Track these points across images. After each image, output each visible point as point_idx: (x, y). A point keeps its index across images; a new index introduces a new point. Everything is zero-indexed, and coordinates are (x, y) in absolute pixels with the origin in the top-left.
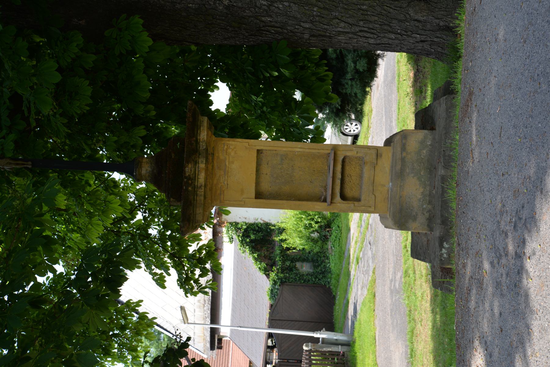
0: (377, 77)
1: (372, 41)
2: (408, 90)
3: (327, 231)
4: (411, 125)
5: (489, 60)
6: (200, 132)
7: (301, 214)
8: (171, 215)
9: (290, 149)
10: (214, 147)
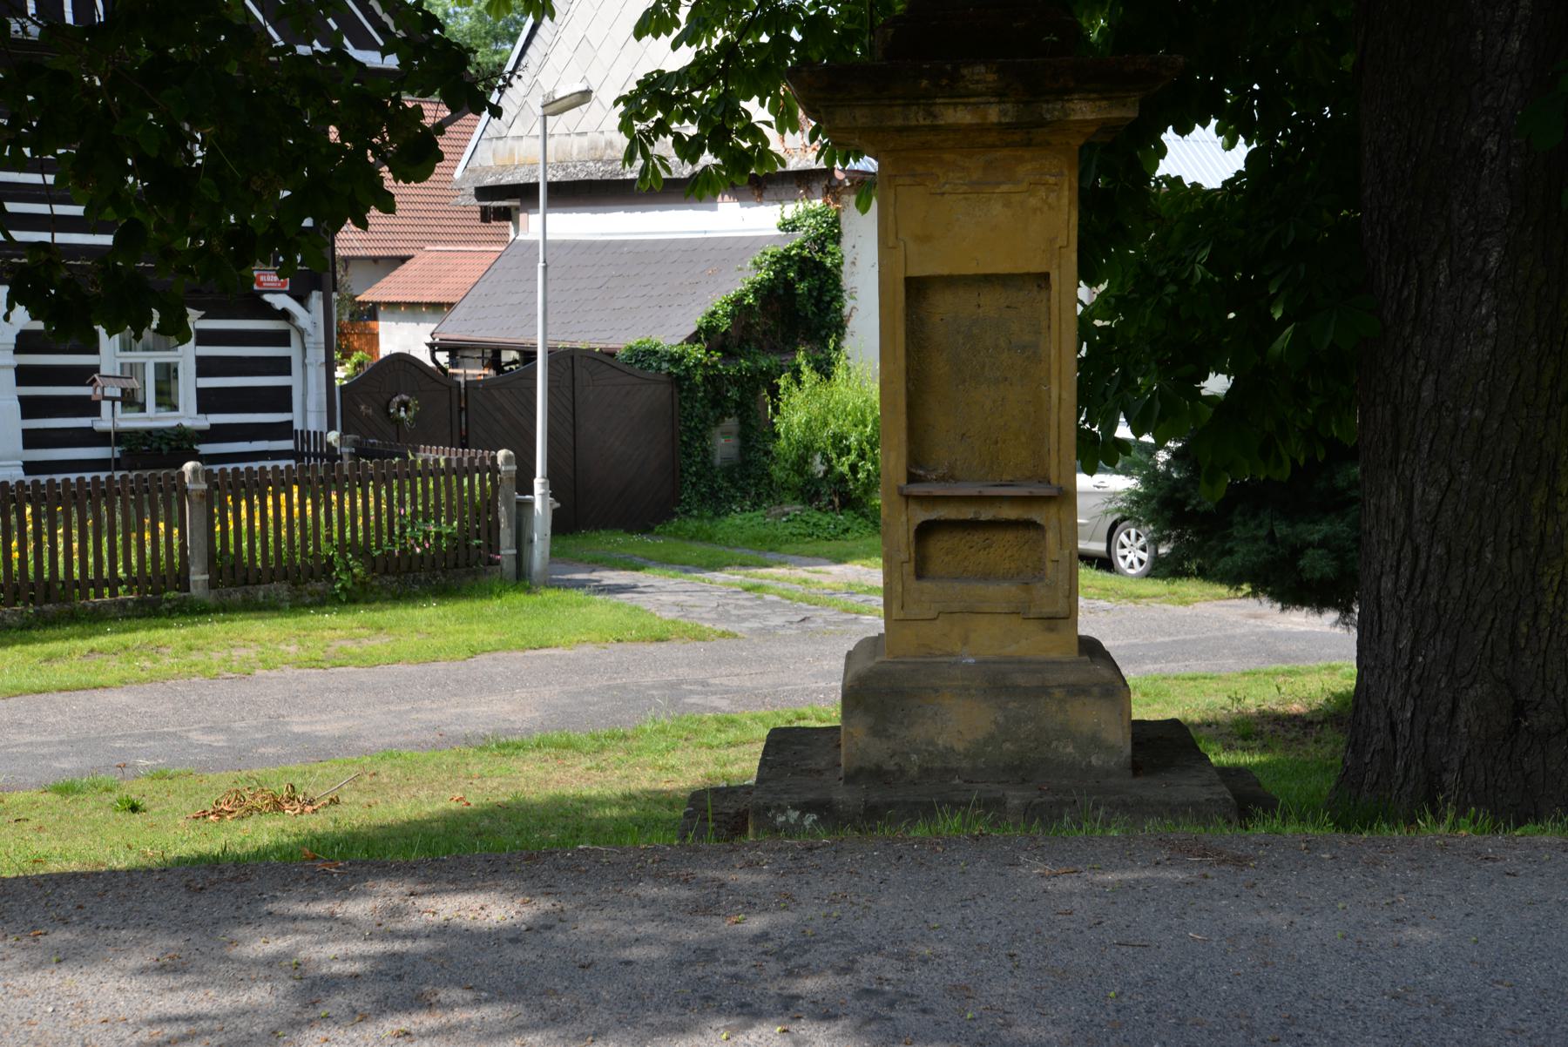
0: (1283, 609)
1: (1387, 584)
2: (1249, 701)
3: (827, 500)
4: (1141, 711)
5: (1340, 905)
6: (1094, 100)
7: (874, 422)
8: (849, 37)
9: (1054, 371)
10: (1049, 144)
